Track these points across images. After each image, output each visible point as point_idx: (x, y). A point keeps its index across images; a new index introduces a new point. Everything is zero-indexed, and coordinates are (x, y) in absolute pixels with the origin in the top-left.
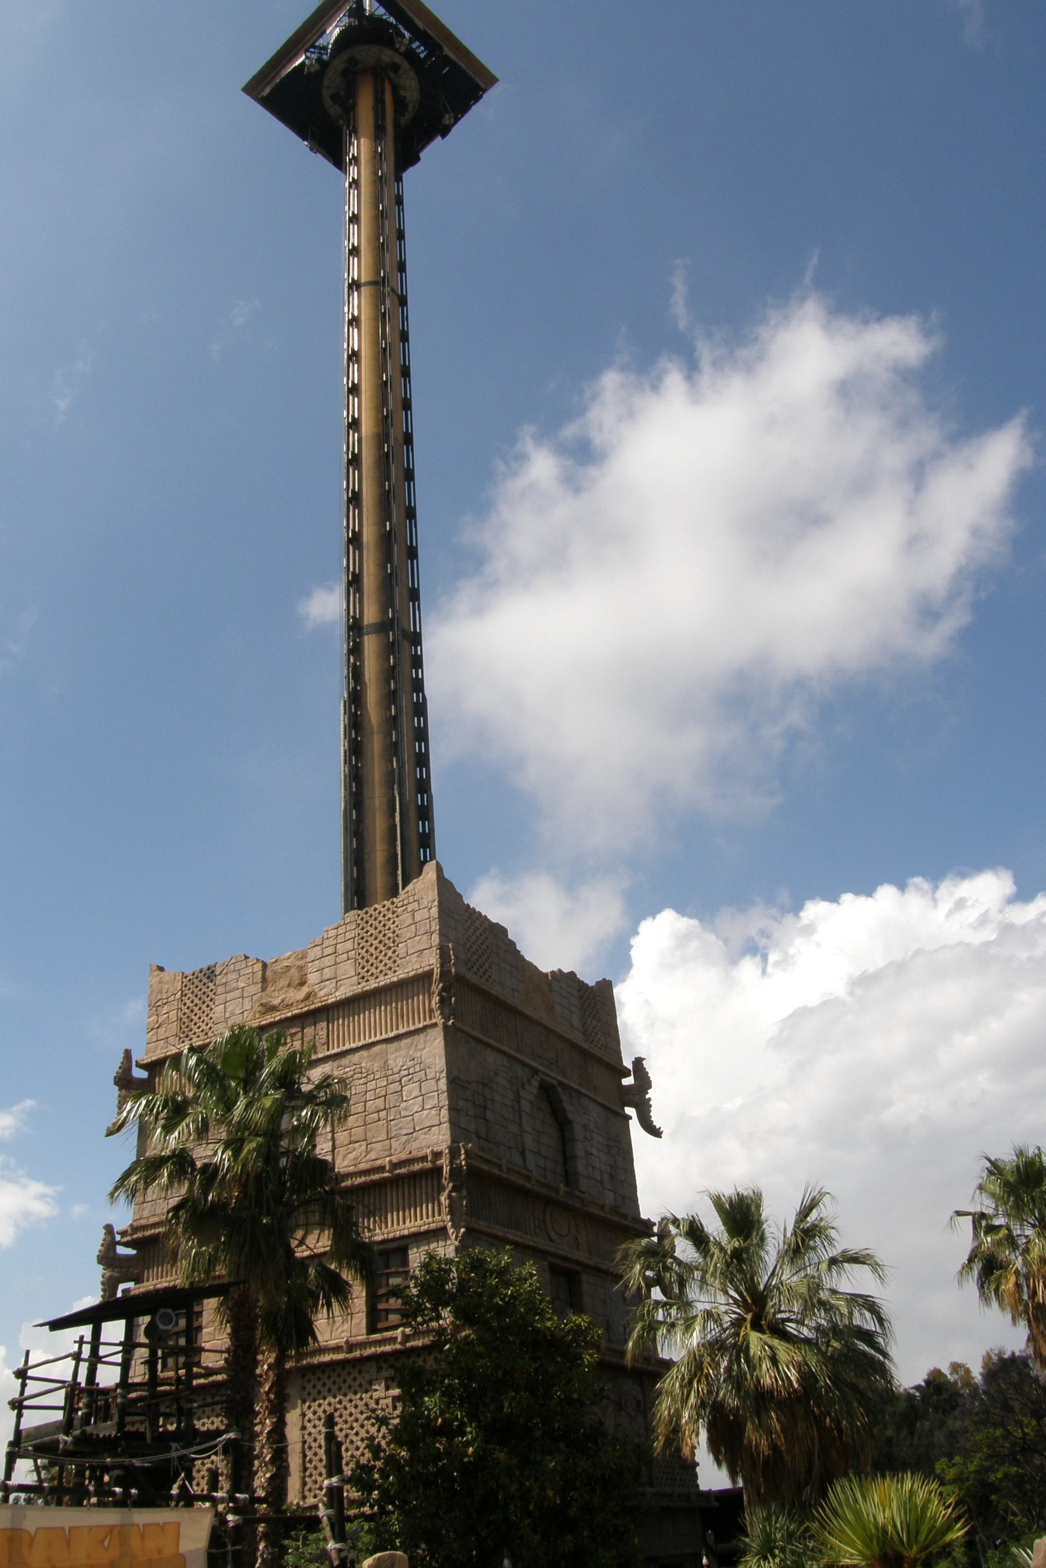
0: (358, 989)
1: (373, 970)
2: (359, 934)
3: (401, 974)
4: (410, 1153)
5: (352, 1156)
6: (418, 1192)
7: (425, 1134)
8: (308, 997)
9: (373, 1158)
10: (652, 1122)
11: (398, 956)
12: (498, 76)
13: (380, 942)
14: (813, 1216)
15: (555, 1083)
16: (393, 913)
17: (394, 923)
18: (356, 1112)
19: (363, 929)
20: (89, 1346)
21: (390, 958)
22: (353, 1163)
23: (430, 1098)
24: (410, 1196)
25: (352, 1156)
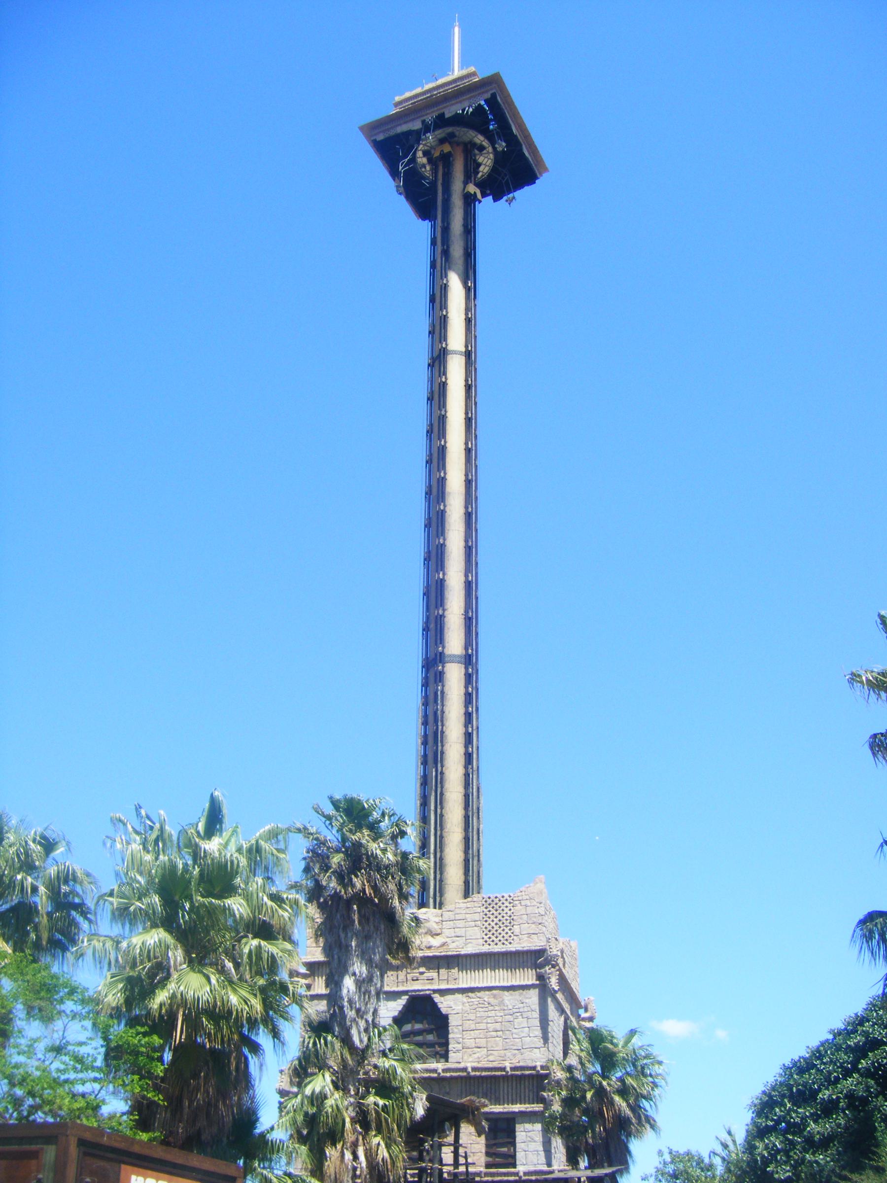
0: (486, 949)
1: (493, 938)
2: (483, 912)
3: (512, 948)
4: (519, 1062)
5: (476, 1056)
6: (522, 1086)
7: (530, 1051)
8: (444, 944)
9: (492, 1060)
10: (400, 1012)
11: (513, 933)
12: (496, 203)
13: (500, 920)
14: (648, 1126)
15: (428, 992)
16: (510, 903)
17: (510, 910)
18: (479, 1028)
19: (486, 908)
20: (460, 1162)
21: (507, 933)
22: (477, 1060)
23: (534, 1030)
24: (516, 1088)
25: (476, 1056)
